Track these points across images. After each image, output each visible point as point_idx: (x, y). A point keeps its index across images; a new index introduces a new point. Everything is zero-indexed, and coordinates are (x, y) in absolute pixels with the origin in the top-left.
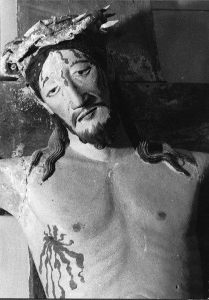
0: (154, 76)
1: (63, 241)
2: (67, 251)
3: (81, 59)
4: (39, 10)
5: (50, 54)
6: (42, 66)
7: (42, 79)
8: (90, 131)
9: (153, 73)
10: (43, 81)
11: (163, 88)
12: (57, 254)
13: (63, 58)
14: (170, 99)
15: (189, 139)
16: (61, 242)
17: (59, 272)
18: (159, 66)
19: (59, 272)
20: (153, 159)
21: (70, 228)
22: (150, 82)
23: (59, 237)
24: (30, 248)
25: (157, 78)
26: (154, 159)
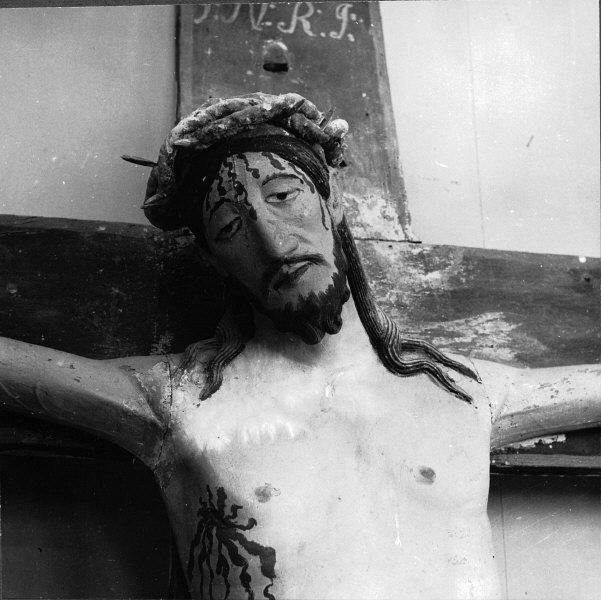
0: (401, 232)
2: (243, 541)
3: (283, 172)
7: (208, 206)
8: (295, 309)
9: (399, 227)
11: (416, 251)
12: (224, 547)
14: (427, 271)
16: (232, 521)
17: (226, 581)
18: (409, 217)
19: (226, 581)
21: (263, 495)
23: (228, 512)
25: (406, 236)
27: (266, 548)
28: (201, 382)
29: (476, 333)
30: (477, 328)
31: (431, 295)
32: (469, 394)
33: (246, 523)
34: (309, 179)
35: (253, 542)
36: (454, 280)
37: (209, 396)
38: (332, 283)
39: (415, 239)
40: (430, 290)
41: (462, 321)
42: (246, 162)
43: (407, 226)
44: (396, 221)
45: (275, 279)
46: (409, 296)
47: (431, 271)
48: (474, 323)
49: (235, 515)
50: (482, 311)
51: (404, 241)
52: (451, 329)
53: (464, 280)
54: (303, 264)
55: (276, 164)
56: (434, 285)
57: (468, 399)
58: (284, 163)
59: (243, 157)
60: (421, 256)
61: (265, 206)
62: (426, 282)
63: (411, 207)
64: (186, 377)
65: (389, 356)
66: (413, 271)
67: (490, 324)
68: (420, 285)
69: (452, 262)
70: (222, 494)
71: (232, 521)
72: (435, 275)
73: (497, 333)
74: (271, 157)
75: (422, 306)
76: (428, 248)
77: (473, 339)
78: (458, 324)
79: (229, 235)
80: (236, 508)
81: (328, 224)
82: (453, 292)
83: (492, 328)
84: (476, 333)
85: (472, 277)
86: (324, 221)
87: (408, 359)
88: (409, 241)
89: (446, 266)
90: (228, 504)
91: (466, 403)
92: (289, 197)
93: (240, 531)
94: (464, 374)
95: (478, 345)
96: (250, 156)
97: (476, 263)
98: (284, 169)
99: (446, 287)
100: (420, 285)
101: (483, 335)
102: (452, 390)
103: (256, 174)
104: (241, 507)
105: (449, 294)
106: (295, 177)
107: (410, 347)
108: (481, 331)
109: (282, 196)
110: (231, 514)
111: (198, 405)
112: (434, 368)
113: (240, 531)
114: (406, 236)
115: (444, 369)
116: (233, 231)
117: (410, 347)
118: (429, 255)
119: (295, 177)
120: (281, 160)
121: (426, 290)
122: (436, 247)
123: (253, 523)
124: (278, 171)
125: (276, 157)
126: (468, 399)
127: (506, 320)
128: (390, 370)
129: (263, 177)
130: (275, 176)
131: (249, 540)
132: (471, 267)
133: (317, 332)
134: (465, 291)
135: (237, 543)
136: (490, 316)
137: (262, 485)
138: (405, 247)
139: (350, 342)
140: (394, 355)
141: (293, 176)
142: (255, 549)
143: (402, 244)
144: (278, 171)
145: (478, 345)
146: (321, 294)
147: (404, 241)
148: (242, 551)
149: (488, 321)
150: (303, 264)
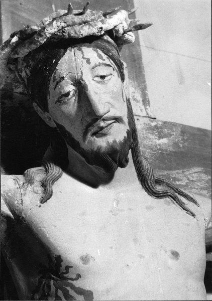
0: (144, 110)
1: (68, 275)
2: (73, 287)
3: (104, 62)
4: (23, 17)
5: (68, 51)
6: (56, 63)
7: (54, 79)
9: (143, 107)
10: (55, 82)
11: (153, 124)
13: (85, 57)
14: (160, 137)
15: (180, 182)
16: (65, 275)
18: (149, 101)
20: (158, 194)
21: (85, 259)
22: (140, 116)
23: (63, 269)
24: (195, 206)
25: (147, 114)
26: (160, 194)
27: (87, 291)
28: (40, 192)
29: (188, 179)
30: (189, 176)
31: (162, 153)
32: (193, 211)
33: (74, 277)
34: (116, 68)
35: (79, 287)
36: (176, 144)
37: (46, 201)
38: (126, 135)
39: (153, 117)
40: (162, 150)
41: (181, 171)
42: (82, 53)
43: (148, 107)
44: (141, 102)
45: (93, 130)
46: (149, 153)
47: (163, 138)
48: (187, 173)
49: (67, 272)
50: (194, 166)
51: (145, 117)
52: (174, 176)
53: (181, 146)
54: (110, 122)
55: (100, 57)
56: (164, 147)
57: (193, 215)
58: (105, 56)
59: (80, 50)
60: (156, 127)
61: (93, 82)
62: (159, 145)
63: (150, 96)
64: (30, 189)
65: (148, 185)
66: (151, 136)
67: (195, 175)
68: (156, 146)
69: (174, 134)
70: (59, 259)
71: (65, 275)
72: (164, 141)
73: (200, 181)
74: (97, 52)
75: (157, 160)
76: (160, 123)
77: (187, 183)
78: (178, 173)
79: (66, 99)
80: (68, 268)
81: (125, 99)
82: (175, 152)
83: (197, 177)
84: (188, 179)
85: (186, 144)
86: (123, 96)
87: (159, 188)
88: (149, 117)
89: (172, 135)
90: (63, 265)
91: (192, 217)
92: (106, 79)
93: (70, 281)
94: (189, 200)
95: (189, 187)
96: (85, 49)
97: (188, 135)
98: (104, 60)
99: (171, 149)
100: (156, 146)
101: (192, 181)
102: (184, 209)
103: (88, 61)
104: (72, 267)
105: (173, 154)
106: (111, 67)
107: (159, 182)
108: (191, 179)
109: (103, 77)
110: (65, 271)
111: (40, 206)
112: (175, 194)
113: (70, 281)
114: (147, 114)
115: (179, 197)
116: (69, 97)
117: (159, 182)
118: (161, 128)
119: (111, 67)
120: (103, 55)
121: (159, 150)
122: (165, 123)
123: (79, 276)
124: (101, 61)
125: (100, 52)
126: (193, 215)
127: (206, 173)
128: (149, 194)
129: (93, 64)
130: (100, 64)
131: (77, 286)
132: (185, 138)
133: (115, 165)
134: (182, 152)
135: (68, 288)
136: (196, 169)
137: (85, 254)
138: (147, 120)
139: (126, 175)
140: (152, 185)
141: (109, 66)
142: (80, 291)
143: (145, 119)
144: (101, 61)
145: (189, 187)
146: (120, 142)
147: (145, 117)
148: (72, 293)
149: (195, 172)
150: (110, 122)
